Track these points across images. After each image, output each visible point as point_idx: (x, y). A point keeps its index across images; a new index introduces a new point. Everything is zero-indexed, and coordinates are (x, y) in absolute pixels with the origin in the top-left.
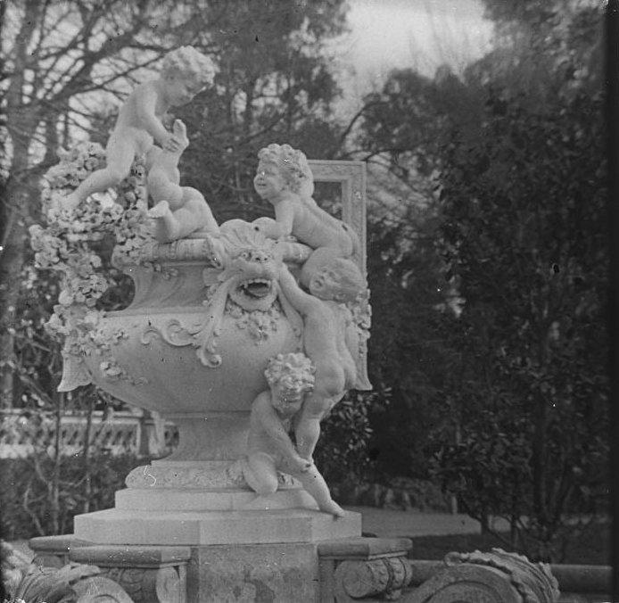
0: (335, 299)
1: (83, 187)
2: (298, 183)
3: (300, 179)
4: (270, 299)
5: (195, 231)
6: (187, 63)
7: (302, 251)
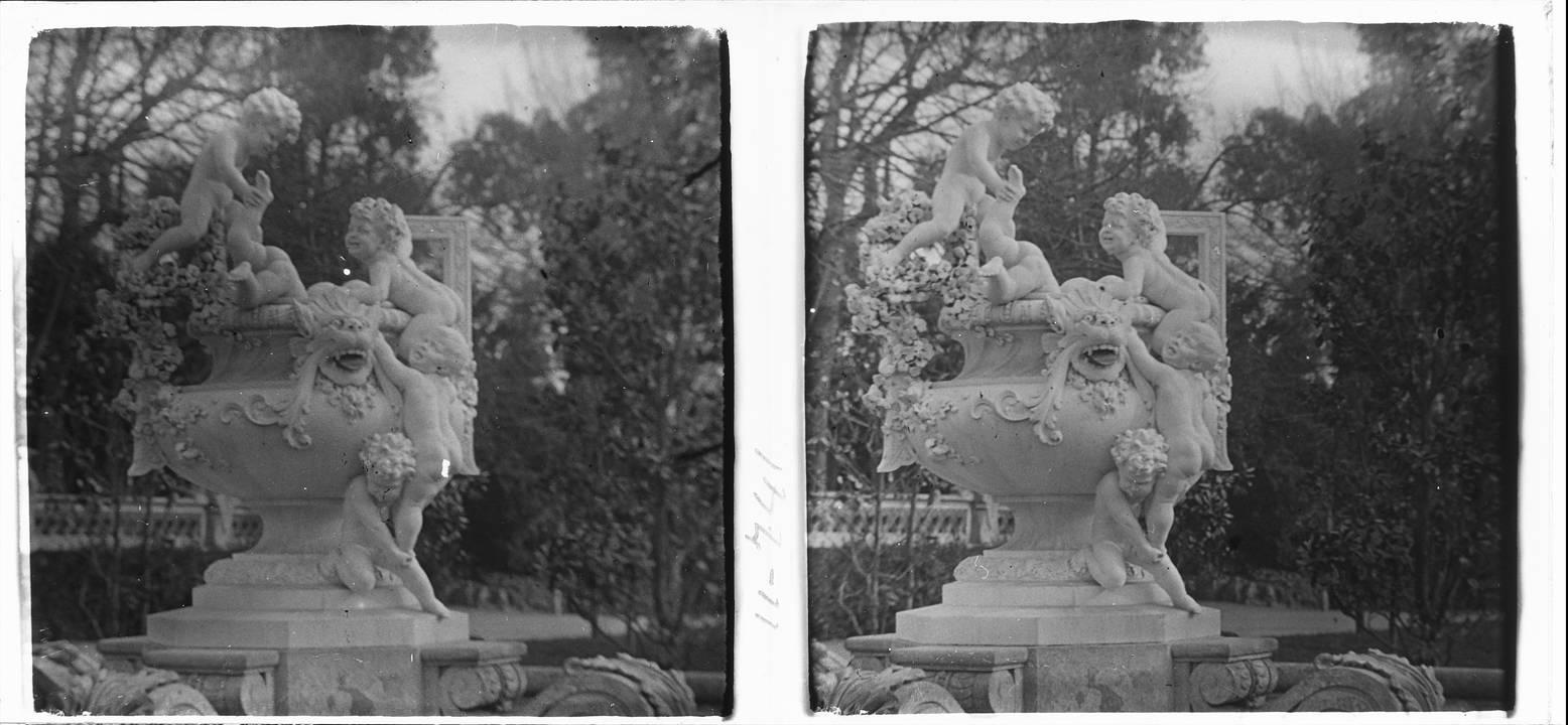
0: (1190, 368)
1: (906, 241)
2: (1149, 237)
3: (1151, 233)
4: (1117, 367)
5: (1033, 291)
6: (1024, 101)
7: (1154, 313)
